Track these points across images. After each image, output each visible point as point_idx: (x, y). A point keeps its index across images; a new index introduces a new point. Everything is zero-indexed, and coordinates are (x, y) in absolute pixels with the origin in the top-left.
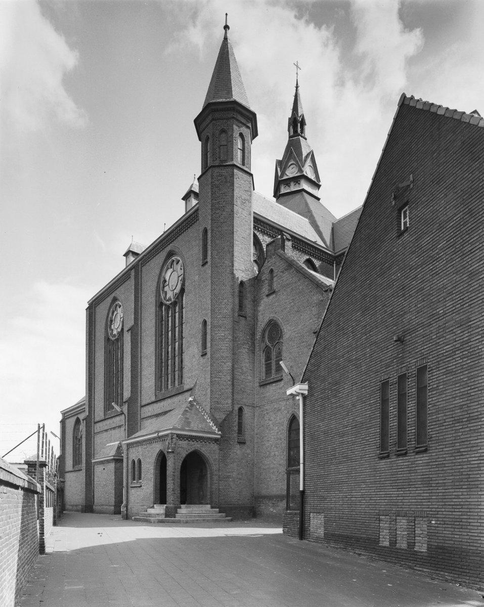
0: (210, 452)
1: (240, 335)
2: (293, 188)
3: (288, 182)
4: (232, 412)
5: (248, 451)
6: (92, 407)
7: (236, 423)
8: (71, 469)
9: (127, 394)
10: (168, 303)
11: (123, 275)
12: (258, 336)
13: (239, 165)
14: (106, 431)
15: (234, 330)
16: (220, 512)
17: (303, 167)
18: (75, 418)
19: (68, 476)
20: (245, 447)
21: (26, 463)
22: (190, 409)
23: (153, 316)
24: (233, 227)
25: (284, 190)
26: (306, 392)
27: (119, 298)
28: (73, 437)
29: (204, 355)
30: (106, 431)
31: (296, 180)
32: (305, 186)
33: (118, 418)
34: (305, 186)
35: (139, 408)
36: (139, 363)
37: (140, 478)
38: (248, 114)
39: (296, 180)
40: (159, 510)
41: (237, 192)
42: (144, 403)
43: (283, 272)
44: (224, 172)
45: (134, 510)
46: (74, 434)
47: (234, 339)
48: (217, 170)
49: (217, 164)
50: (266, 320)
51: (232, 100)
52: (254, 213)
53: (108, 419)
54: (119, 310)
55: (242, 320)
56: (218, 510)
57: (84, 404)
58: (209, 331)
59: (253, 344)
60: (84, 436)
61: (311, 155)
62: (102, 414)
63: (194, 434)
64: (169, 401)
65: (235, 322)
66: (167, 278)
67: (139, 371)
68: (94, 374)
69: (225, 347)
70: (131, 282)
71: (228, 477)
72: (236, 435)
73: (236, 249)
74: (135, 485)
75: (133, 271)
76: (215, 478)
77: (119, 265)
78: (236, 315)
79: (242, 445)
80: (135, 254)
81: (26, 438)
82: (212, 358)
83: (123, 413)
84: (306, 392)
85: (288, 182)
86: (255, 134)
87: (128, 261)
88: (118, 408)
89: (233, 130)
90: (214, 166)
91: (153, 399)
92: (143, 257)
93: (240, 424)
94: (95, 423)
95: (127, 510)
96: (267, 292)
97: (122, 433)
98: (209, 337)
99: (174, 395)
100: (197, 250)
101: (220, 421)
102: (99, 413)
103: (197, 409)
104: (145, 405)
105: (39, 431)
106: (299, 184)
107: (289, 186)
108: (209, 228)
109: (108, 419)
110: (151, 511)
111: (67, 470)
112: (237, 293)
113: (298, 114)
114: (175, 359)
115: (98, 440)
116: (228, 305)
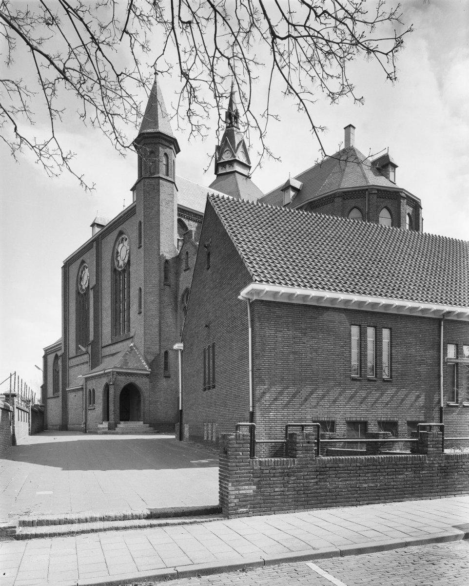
0: (143, 384)
1: (166, 299)
2: (228, 169)
3: (224, 165)
4: (159, 354)
5: (173, 383)
6: (66, 346)
7: (163, 363)
8: (52, 396)
9: (91, 338)
10: (120, 269)
11: (88, 244)
12: (179, 299)
13: (163, 177)
14: (77, 365)
15: (160, 296)
16: (150, 426)
17: (236, 153)
18: (54, 354)
19: (49, 401)
20: (170, 379)
21: (4, 394)
22: (129, 353)
23: (109, 278)
24: (159, 222)
25: (221, 171)
26: (182, 348)
27: (86, 261)
28: (53, 370)
29: (140, 313)
30: (77, 365)
31: (231, 163)
32: (237, 168)
33: (84, 357)
34: (237, 168)
35: (100, 348)
36: (100, 314)
37: (94, 403)
38: (170, 139)
39: (231, 163)
40: (105, 425)
41: (162, 196)
42: (104, 345)
43: (193, 255)
44: (153, 182)
45: (91, 426)
46: (54, 367)
47: (161, 302)
48: (147, 180)
49: (148, 176)
50: (184, 288)
51: (157, 130)
52: (178, 205)
53: (79, 356)
54: (87, 270)
55: (167, 288)
56: (148, 425)
57: (61, 344)
58: (143, 296)
59: (176, 304)
60: (61, 369)
61: (242, 142)
62: (74, 352)
63: (129, 371)
64: (120, 344)
65: (161, 290)
66: (119, 251)
67: (100, 320)
68: (68, 319)
69: (153, 308)
70: (94, 250)
71: (157, 402)
72: (162, 371)
73: (162, 237)
74: (91, 408)
75: (95, 243)
76: (147, 402)
77: (86, 235)
78: (162, 284)
79: (167, 379)
80: (99, 225)
81: (320, 139)
82: (145, 315)
83: (88, 353)
84: (182, 348)
85: (224, 165)
86: (178, 150)
87: (94, 231)
88: (84, 349)
89: (159, 151)
90: (146, 178)
91: (110, 342)
92: (107, 229)
93: (166, 364)
94: (69, 359)
95: (86, 426)
96: (184, 268)
97: (86, 368)
98: (143, 300)
99: (124, 340)
100: (136, 234)
101: (150, 361)
102: (72, 352)
103: (135, 352)
104: (104, 347)
105: (11, 377)
106: (233, 166)
107: (225, 168)
108: (142, 221)
109: (79, 356)
110: (100, 426)
111: (48, 396)
112: (163, 269)
113: (232, 110)
114: (125, 312)
115: (72, 372)
116: (156, 278)
